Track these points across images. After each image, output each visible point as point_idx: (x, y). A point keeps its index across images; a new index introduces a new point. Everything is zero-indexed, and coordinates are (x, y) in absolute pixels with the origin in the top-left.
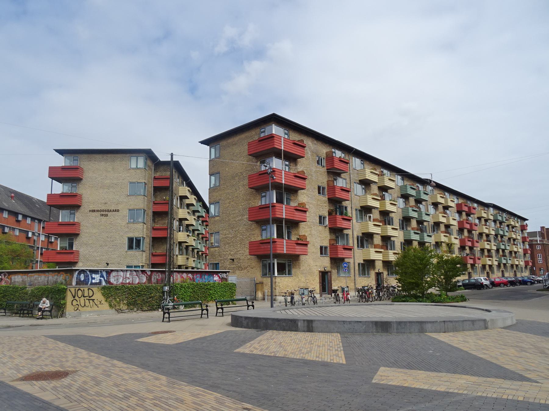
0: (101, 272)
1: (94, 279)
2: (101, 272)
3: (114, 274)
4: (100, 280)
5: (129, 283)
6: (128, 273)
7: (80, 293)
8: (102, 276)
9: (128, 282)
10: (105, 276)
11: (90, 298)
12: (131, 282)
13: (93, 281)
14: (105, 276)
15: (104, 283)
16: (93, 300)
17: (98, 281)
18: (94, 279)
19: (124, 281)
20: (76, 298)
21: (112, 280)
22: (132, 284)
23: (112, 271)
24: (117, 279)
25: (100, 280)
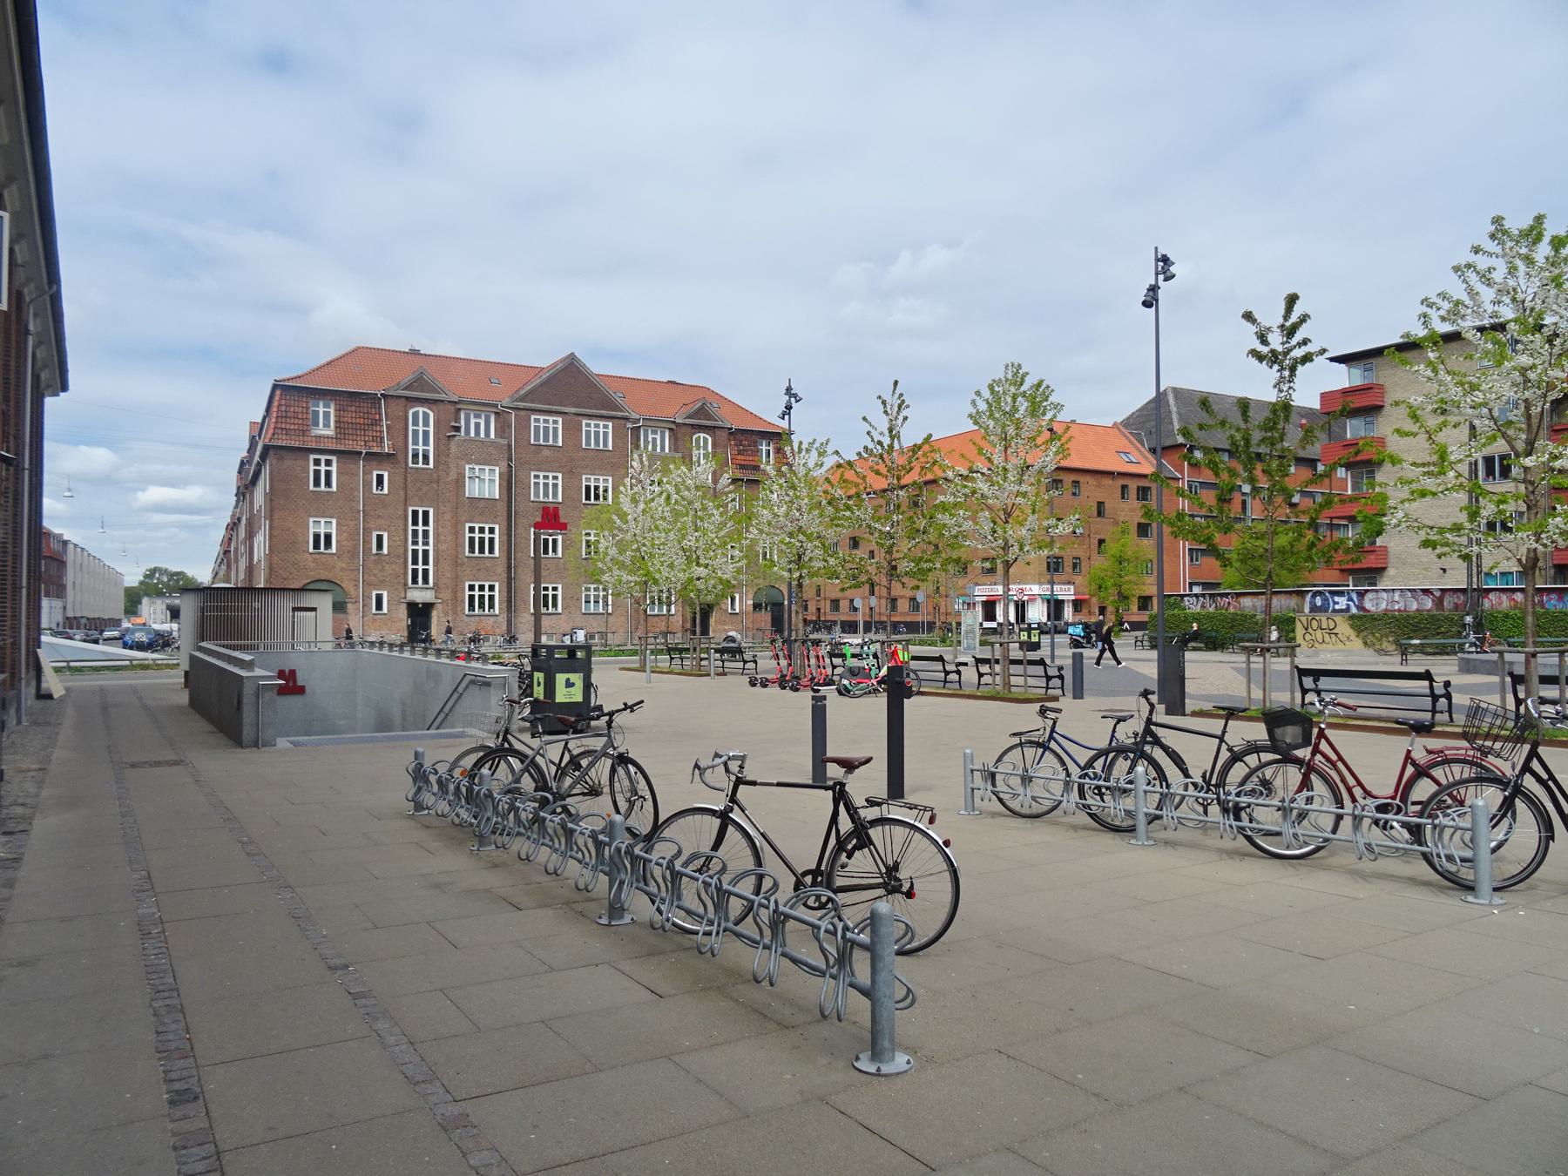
0: (1348, 593)
1: (1338, 603)
2: (1348, 593)
3: (1369, 596)
4: (1348, 606)
5: (1399, 610)
6: (1397, 596)
7: (1315, 624)
8: (1350, 599)
9: (1396, 608)
10: (1355, 599)
11: (1331, 632)
12: (1402, 609)
13: (1337, 607)
14: (1355, 599)
15: (1354, 610)
16: (1336, 634)
17: (1344, 607)
18: (1338, 603)
19: (1389, 607)
20: (1310, 630)
21: (1368, 605)
22: (1405, 611)
23: (1367, 591)
24: (1377, 604)
25: (1348, 606)
